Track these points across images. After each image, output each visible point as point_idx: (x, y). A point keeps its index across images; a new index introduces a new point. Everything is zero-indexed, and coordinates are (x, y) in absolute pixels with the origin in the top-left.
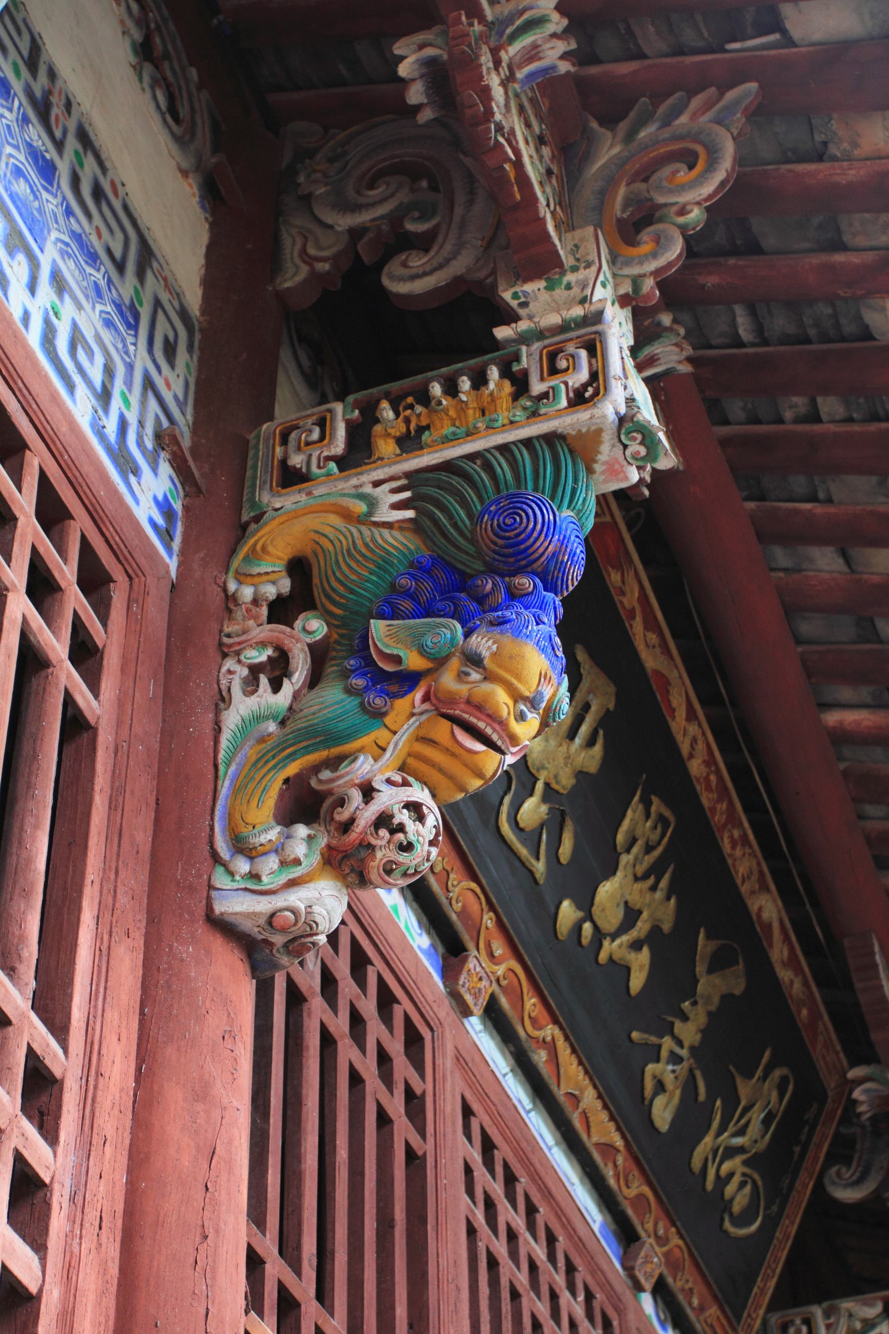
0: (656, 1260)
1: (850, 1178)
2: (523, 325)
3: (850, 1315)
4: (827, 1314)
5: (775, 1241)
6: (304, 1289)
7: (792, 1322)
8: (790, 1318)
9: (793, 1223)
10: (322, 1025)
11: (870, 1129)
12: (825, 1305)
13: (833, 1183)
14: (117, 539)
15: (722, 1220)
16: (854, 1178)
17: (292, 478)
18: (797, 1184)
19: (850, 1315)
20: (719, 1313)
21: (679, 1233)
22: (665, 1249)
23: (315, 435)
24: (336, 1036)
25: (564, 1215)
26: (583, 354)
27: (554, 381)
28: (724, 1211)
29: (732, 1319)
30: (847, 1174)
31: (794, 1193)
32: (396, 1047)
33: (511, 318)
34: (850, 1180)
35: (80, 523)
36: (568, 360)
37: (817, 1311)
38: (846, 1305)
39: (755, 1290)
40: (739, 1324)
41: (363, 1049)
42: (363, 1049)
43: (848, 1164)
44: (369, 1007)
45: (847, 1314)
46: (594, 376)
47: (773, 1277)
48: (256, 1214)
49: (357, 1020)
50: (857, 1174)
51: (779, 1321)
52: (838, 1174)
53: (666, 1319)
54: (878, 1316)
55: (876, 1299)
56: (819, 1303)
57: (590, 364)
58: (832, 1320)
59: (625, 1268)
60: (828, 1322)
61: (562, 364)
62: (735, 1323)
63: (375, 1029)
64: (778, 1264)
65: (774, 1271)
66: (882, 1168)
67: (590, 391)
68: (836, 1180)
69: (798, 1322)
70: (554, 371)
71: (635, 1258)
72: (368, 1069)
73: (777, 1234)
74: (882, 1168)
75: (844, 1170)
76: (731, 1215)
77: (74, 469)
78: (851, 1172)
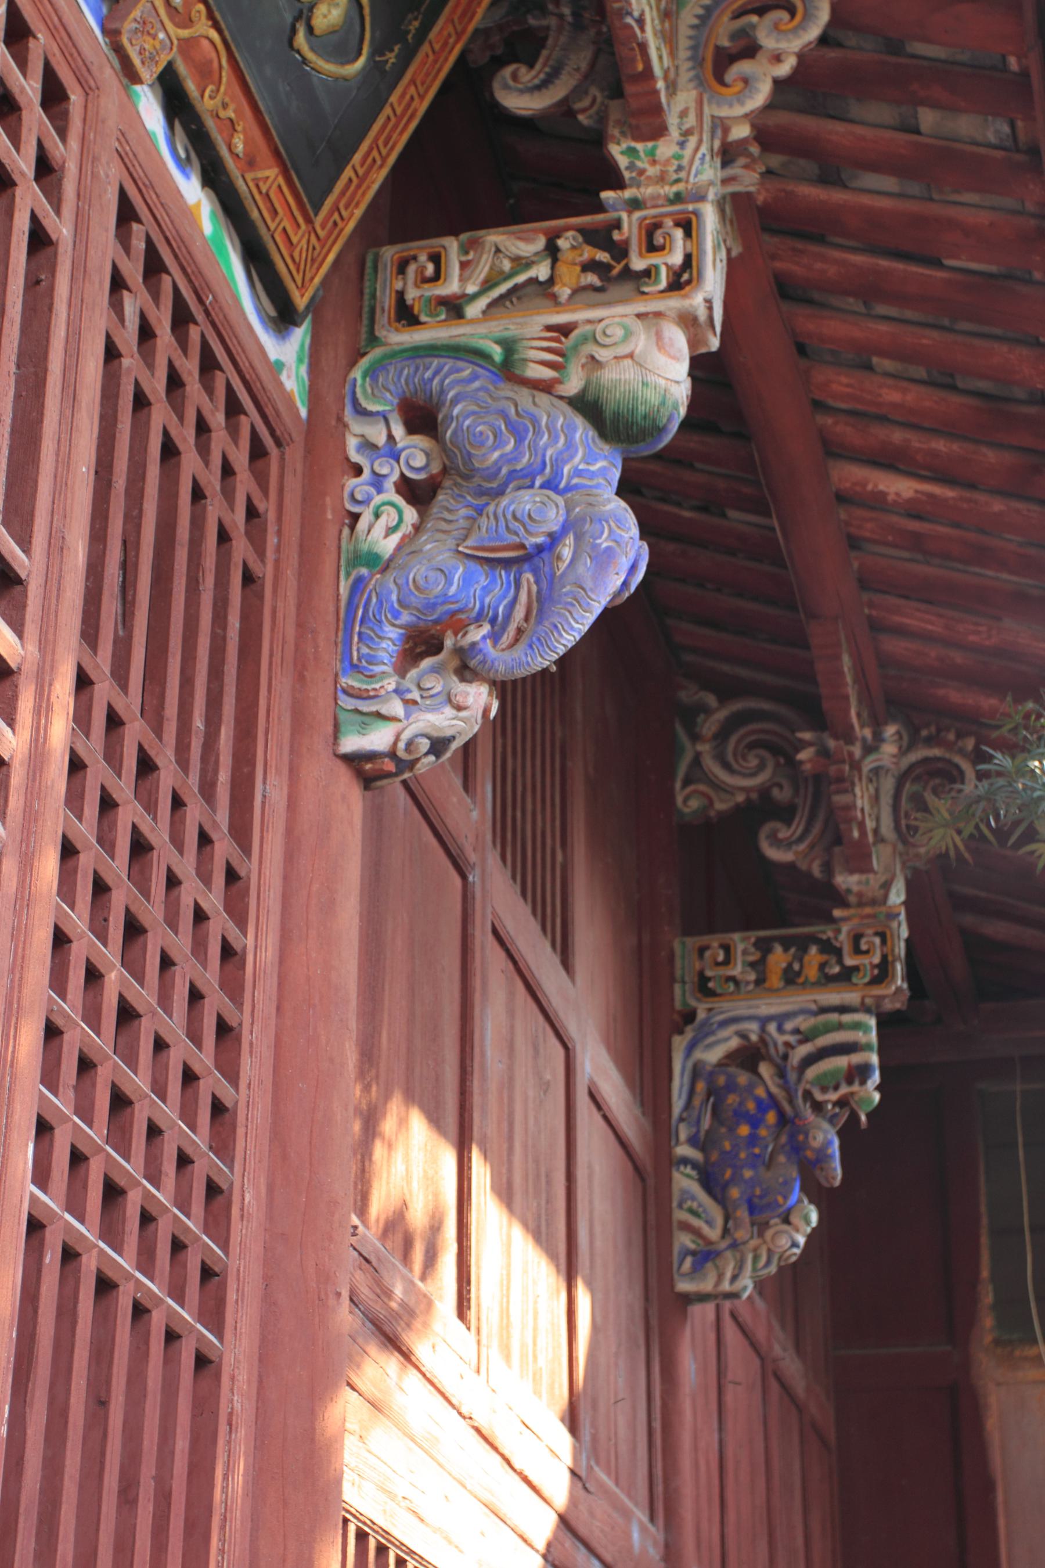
0: (161, 35)
1: (529, 81)
2: (628, 194)
3: (498, 251)
4: (465, 250)
5: (387, 111)
6: (129, 705)
7: (415, 258)
8: (412, 253)
9: (422, 97)
10: (137, 384)
11: (570, 19)
12: (464, 237)
13: (506, 87)
14: (56, 19)
15: (294, 31)
16: (536, 81)
17: (406, 316)
18: (432, 35)
19: (498, 251)
20: (281, 180)
21: (211, 16)
22: (185, 33)
23: (721, 957)
24: (151, 398)
25: (236, 337)
26: (679, 234)
27: (654, 259)
28: (297, 19)
29: (308, 206)
30: (527, 76)
31: (425, 48)
32: (240, 458)
33: (619, 184)
34: (530, 85)
35: (41, 43)
36: (664, 238)
37: (452, 245)
38: (493, 237)
39: (348, 173)
40: (316, 215)
41: (150, 365)
42: (150, 365)
43: (531, 66)
44: (190, 368)
45: (493, 249)
46: (688, 258)
47: (381, 166)
48: (90, 634)
49: (175, 382)
50: (542, 76)
51: (396, 257)
52: (515, 77)
53: (188, 158)
54: (536, 254)
55: (535, 231)
56: (455, 233)
57: (882, 951)
58: (471, 256)
59: (105, 31)
60: (464, 259)
61: (659, 240)
62: (312, 214)
63: (219, 438)
64: (392, 149)
65: (384, 160)
66: (578, 70)
67: (685, 277)
68: (511, 83)
69: (423, 258)
70: (652, 248)
71: (124, 18)
72: (185, 440)
73: (393, 99)
74: (578, 70)
75: (523, 69)
76: (310, 30)
77: (138, 168)
78: (533, 73)
